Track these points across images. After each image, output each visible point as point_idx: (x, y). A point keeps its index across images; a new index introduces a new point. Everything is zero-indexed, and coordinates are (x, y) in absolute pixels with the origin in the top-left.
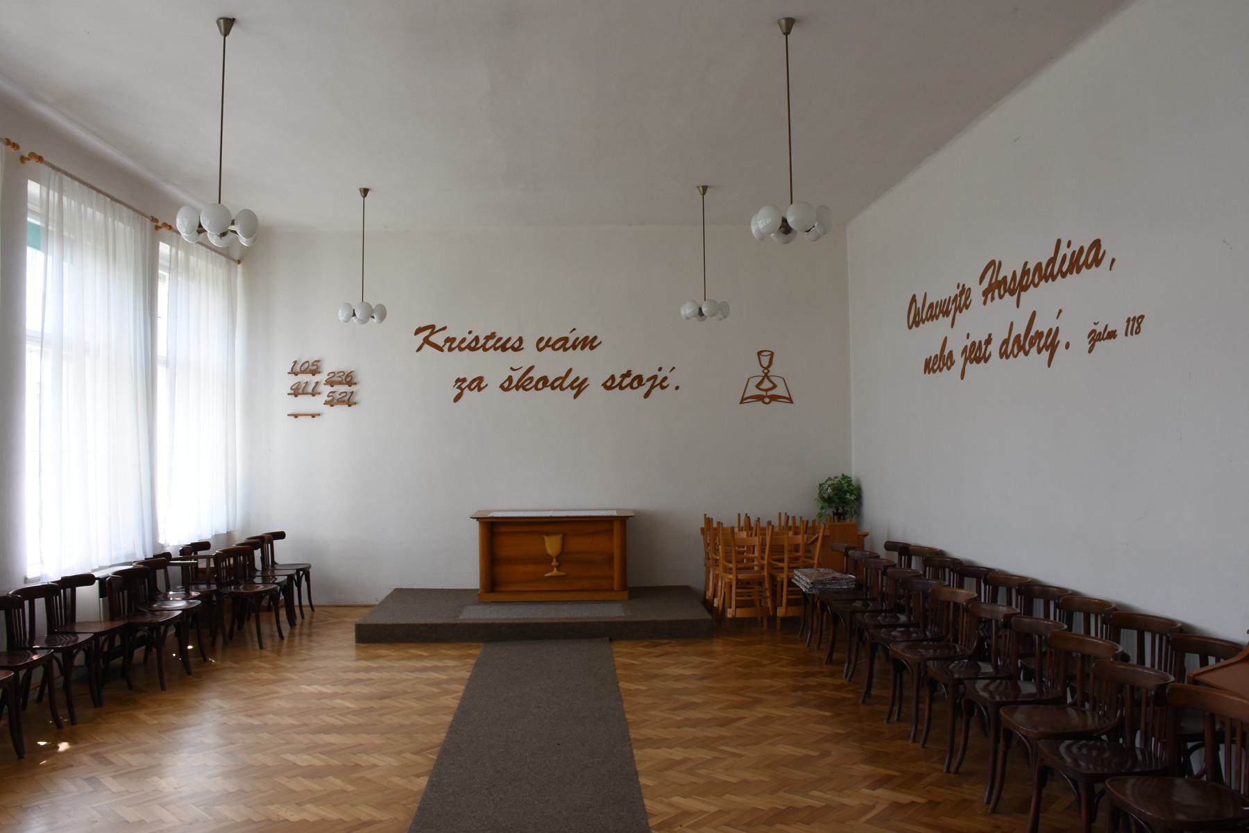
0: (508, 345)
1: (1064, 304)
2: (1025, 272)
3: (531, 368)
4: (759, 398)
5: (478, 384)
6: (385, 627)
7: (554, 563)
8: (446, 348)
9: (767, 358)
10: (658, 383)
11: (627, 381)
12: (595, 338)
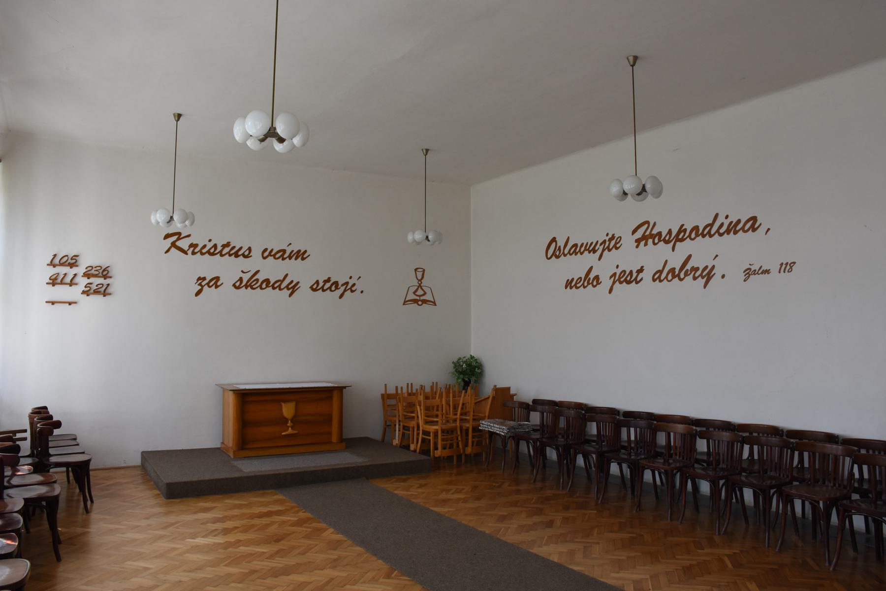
0: (240, 253)
1: (728, 253)
2: (682, 230)
3: (258, 272)
4: (415, 301)
5: (215, 282)
6: (191, 483)
7: (289, 424)
8: (190, 252)
9: (420, 273)
10: (349, 288)
11: (328, 285)
12: (305, 252)
